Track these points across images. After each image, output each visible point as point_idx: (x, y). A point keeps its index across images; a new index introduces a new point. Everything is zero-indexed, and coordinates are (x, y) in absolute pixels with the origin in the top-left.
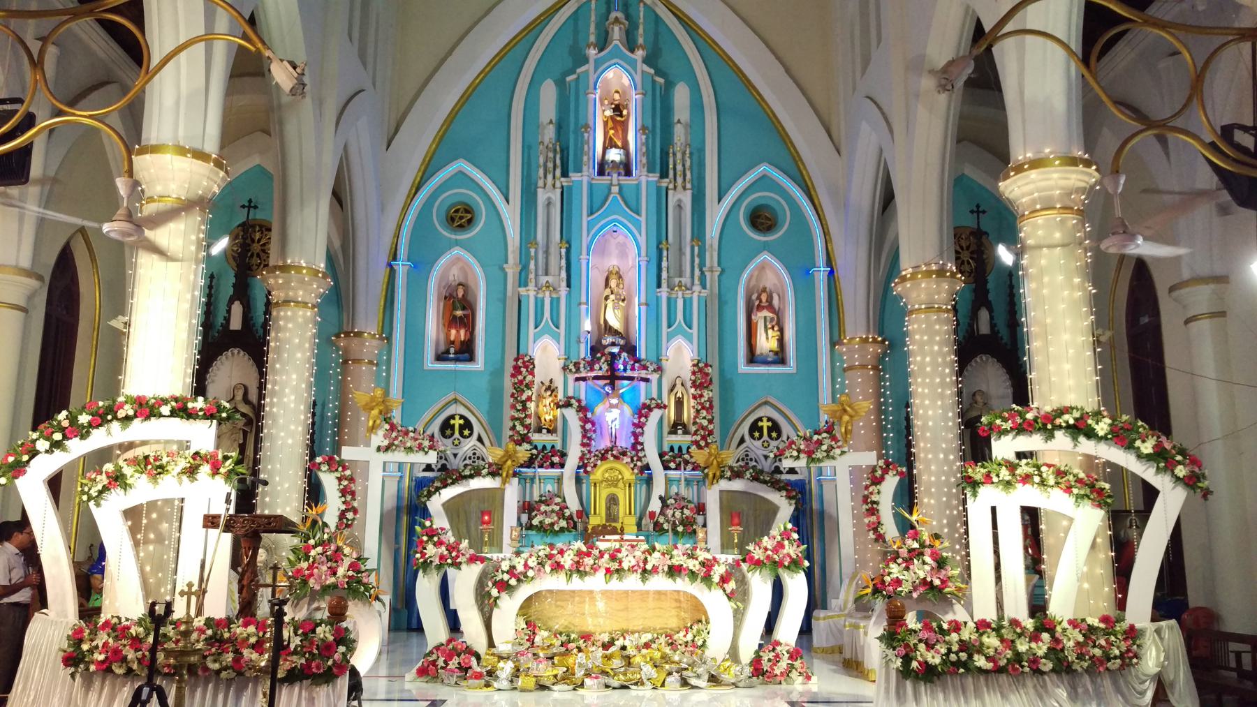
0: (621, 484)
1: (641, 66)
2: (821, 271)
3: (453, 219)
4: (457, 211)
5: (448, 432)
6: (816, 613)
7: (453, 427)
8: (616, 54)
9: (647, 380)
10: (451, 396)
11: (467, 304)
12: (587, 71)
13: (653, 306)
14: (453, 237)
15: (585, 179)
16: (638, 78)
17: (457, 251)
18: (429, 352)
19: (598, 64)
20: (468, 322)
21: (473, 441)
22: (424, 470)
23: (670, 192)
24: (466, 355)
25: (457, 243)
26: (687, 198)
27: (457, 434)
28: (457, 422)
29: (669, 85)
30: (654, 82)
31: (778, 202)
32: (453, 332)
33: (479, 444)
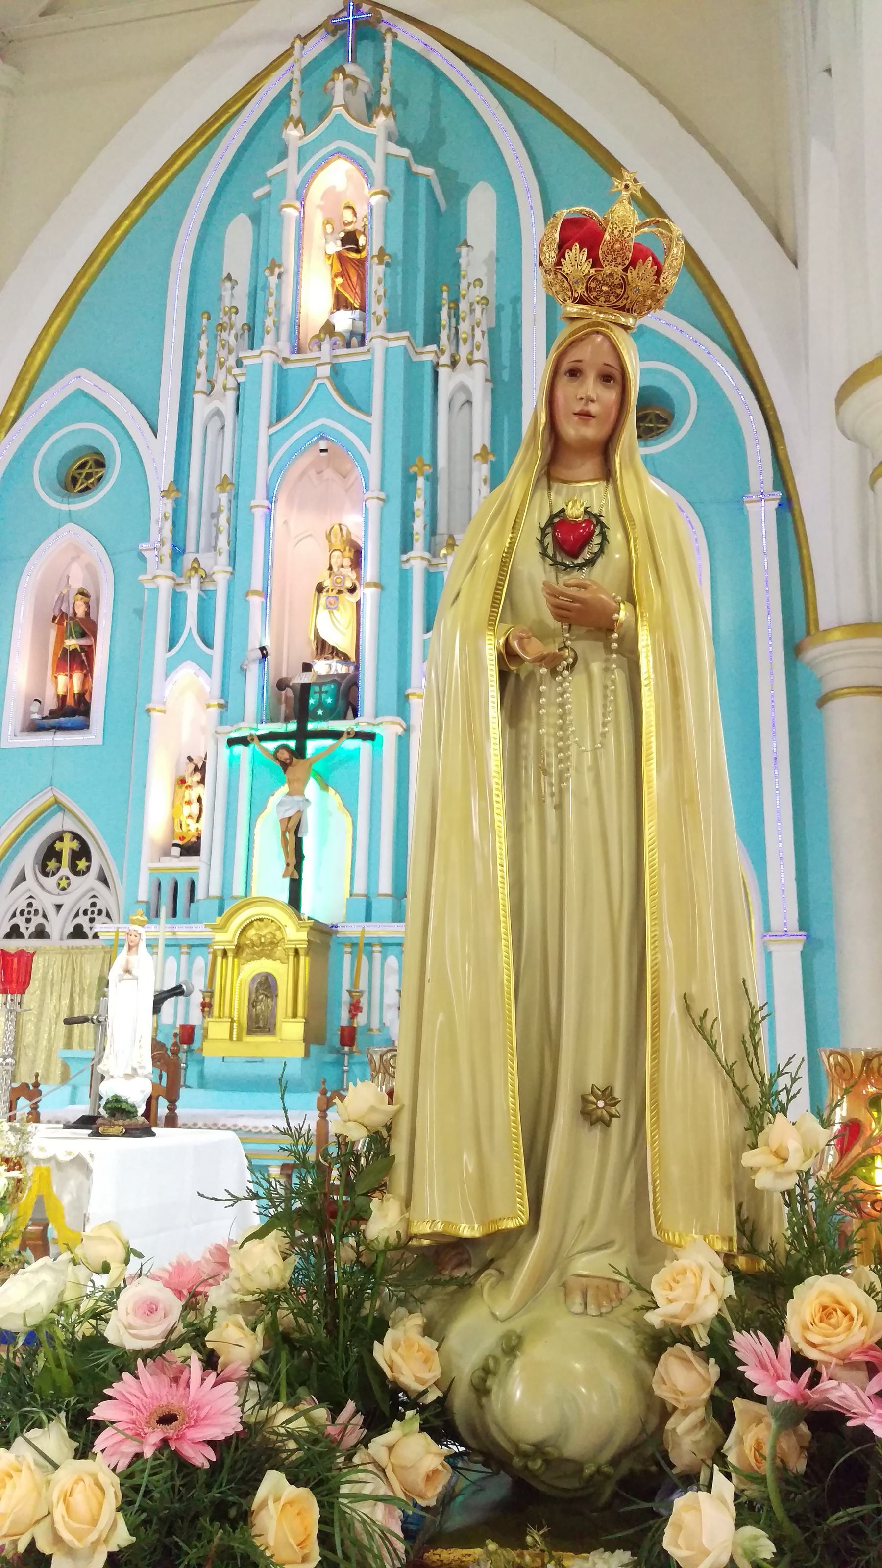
0: (279, 952)
1: (384, 147)
2: (763, 515)
3: (74, 481)
4: (83, 466)
5: (52, 865)
6: (381, 1505)
7: (58, 856)
8: (341, 131)
9: (369, 736)
10: (47, 798)
11: (86, 628)
12: (284, 171)
13: (394, 591)
14: (65, 507)
15: (268, 360)
16: (377, 168)
17: (70, 533)
18: (13, 715)
19: (303, 154)
20: (80, 660)
21: (90, 880)
22: (8, 936)
23: (443, 372)
24: (78, 719)
25: (70, 517)
26: (475, 378)
27: (65, 870)
28: (67, 846)
29: (456, 190)
30: (410, 175)
31: (685, 390)
32: (62, 679)
33: (100, 886)
